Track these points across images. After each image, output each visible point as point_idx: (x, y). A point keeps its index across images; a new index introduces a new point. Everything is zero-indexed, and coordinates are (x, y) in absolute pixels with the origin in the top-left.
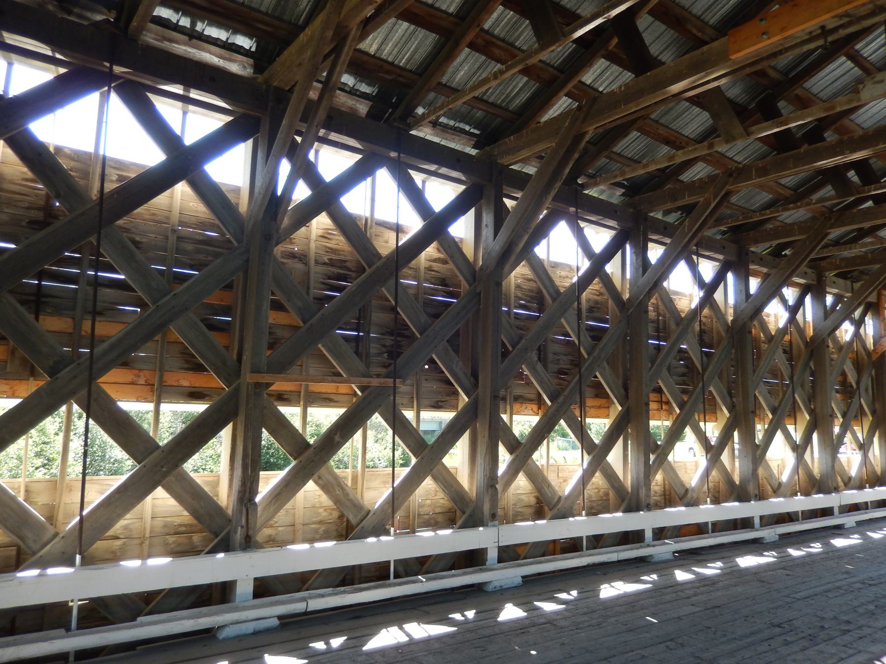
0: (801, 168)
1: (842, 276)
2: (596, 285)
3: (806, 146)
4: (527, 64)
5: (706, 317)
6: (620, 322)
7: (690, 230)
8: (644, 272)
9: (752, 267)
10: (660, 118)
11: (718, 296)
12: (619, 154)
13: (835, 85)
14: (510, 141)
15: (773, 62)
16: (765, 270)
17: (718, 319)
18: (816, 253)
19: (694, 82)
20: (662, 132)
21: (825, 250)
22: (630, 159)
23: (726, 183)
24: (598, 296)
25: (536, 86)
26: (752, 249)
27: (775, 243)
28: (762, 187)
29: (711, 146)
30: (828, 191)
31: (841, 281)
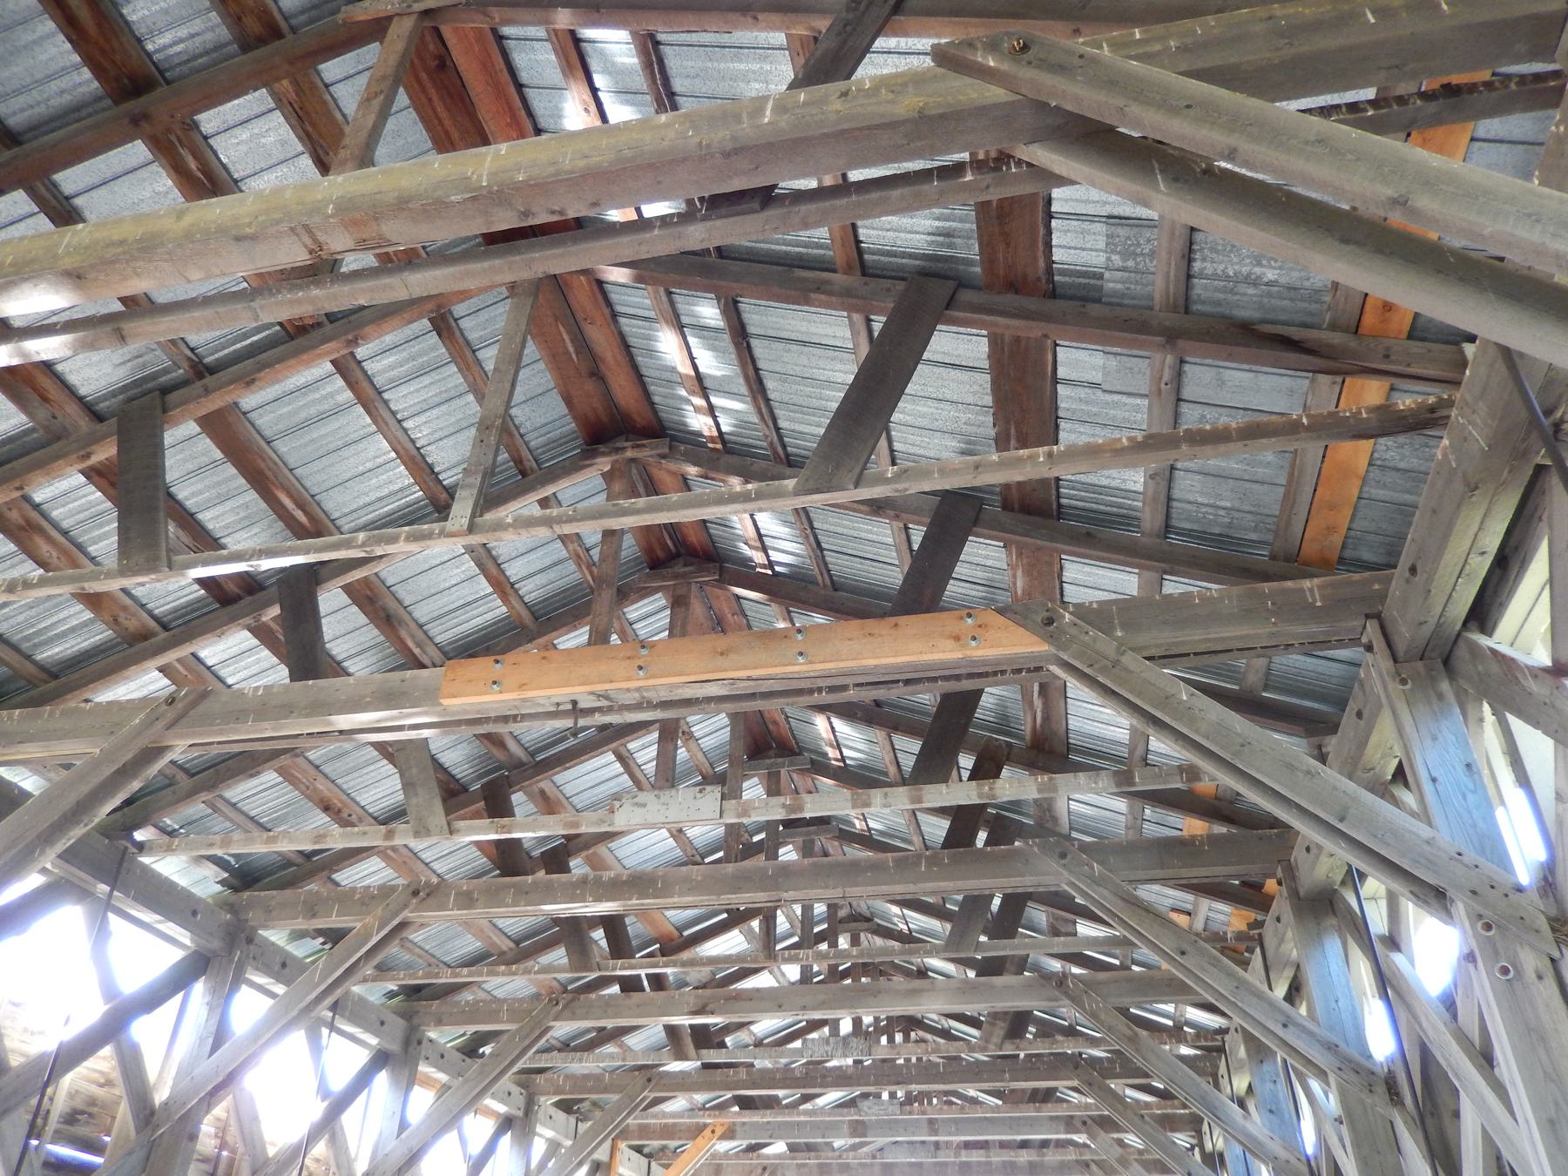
0: (523, 908)
1: (566, 1106)
2: (103, 1061)
3: (541, 874)
4: (83, 589)
5: (317, 1161)
6: (130, 1153)
7: (323, 978)
8: (215, 1047)
9: (424, 1068)
10: (325, 762)
11: (350, 1119)
12: (234, 805)
13: (596, 791)
14: (10, 718)
15: (516, 728)
16: (443, 1077)
17: (338, 1167)
18: (529, 1059)
19: (386, 720)
20: (321, 787)
21: (545, 1056)
22: (252, 818)
23: (406, 906)
24: (101, 1086)
25: (105, 634)
26: (432, 1035)
27: (472, 1029)
28: (467, 925)
29: (389, 835)
30: (559, 956)
31: (560, 1116)
